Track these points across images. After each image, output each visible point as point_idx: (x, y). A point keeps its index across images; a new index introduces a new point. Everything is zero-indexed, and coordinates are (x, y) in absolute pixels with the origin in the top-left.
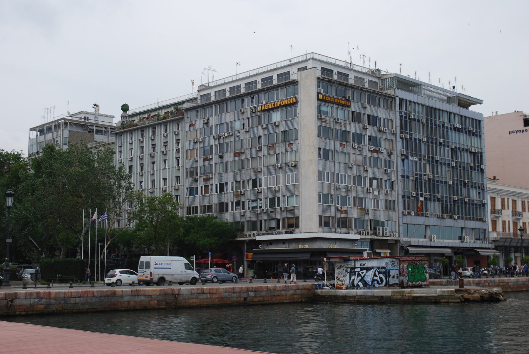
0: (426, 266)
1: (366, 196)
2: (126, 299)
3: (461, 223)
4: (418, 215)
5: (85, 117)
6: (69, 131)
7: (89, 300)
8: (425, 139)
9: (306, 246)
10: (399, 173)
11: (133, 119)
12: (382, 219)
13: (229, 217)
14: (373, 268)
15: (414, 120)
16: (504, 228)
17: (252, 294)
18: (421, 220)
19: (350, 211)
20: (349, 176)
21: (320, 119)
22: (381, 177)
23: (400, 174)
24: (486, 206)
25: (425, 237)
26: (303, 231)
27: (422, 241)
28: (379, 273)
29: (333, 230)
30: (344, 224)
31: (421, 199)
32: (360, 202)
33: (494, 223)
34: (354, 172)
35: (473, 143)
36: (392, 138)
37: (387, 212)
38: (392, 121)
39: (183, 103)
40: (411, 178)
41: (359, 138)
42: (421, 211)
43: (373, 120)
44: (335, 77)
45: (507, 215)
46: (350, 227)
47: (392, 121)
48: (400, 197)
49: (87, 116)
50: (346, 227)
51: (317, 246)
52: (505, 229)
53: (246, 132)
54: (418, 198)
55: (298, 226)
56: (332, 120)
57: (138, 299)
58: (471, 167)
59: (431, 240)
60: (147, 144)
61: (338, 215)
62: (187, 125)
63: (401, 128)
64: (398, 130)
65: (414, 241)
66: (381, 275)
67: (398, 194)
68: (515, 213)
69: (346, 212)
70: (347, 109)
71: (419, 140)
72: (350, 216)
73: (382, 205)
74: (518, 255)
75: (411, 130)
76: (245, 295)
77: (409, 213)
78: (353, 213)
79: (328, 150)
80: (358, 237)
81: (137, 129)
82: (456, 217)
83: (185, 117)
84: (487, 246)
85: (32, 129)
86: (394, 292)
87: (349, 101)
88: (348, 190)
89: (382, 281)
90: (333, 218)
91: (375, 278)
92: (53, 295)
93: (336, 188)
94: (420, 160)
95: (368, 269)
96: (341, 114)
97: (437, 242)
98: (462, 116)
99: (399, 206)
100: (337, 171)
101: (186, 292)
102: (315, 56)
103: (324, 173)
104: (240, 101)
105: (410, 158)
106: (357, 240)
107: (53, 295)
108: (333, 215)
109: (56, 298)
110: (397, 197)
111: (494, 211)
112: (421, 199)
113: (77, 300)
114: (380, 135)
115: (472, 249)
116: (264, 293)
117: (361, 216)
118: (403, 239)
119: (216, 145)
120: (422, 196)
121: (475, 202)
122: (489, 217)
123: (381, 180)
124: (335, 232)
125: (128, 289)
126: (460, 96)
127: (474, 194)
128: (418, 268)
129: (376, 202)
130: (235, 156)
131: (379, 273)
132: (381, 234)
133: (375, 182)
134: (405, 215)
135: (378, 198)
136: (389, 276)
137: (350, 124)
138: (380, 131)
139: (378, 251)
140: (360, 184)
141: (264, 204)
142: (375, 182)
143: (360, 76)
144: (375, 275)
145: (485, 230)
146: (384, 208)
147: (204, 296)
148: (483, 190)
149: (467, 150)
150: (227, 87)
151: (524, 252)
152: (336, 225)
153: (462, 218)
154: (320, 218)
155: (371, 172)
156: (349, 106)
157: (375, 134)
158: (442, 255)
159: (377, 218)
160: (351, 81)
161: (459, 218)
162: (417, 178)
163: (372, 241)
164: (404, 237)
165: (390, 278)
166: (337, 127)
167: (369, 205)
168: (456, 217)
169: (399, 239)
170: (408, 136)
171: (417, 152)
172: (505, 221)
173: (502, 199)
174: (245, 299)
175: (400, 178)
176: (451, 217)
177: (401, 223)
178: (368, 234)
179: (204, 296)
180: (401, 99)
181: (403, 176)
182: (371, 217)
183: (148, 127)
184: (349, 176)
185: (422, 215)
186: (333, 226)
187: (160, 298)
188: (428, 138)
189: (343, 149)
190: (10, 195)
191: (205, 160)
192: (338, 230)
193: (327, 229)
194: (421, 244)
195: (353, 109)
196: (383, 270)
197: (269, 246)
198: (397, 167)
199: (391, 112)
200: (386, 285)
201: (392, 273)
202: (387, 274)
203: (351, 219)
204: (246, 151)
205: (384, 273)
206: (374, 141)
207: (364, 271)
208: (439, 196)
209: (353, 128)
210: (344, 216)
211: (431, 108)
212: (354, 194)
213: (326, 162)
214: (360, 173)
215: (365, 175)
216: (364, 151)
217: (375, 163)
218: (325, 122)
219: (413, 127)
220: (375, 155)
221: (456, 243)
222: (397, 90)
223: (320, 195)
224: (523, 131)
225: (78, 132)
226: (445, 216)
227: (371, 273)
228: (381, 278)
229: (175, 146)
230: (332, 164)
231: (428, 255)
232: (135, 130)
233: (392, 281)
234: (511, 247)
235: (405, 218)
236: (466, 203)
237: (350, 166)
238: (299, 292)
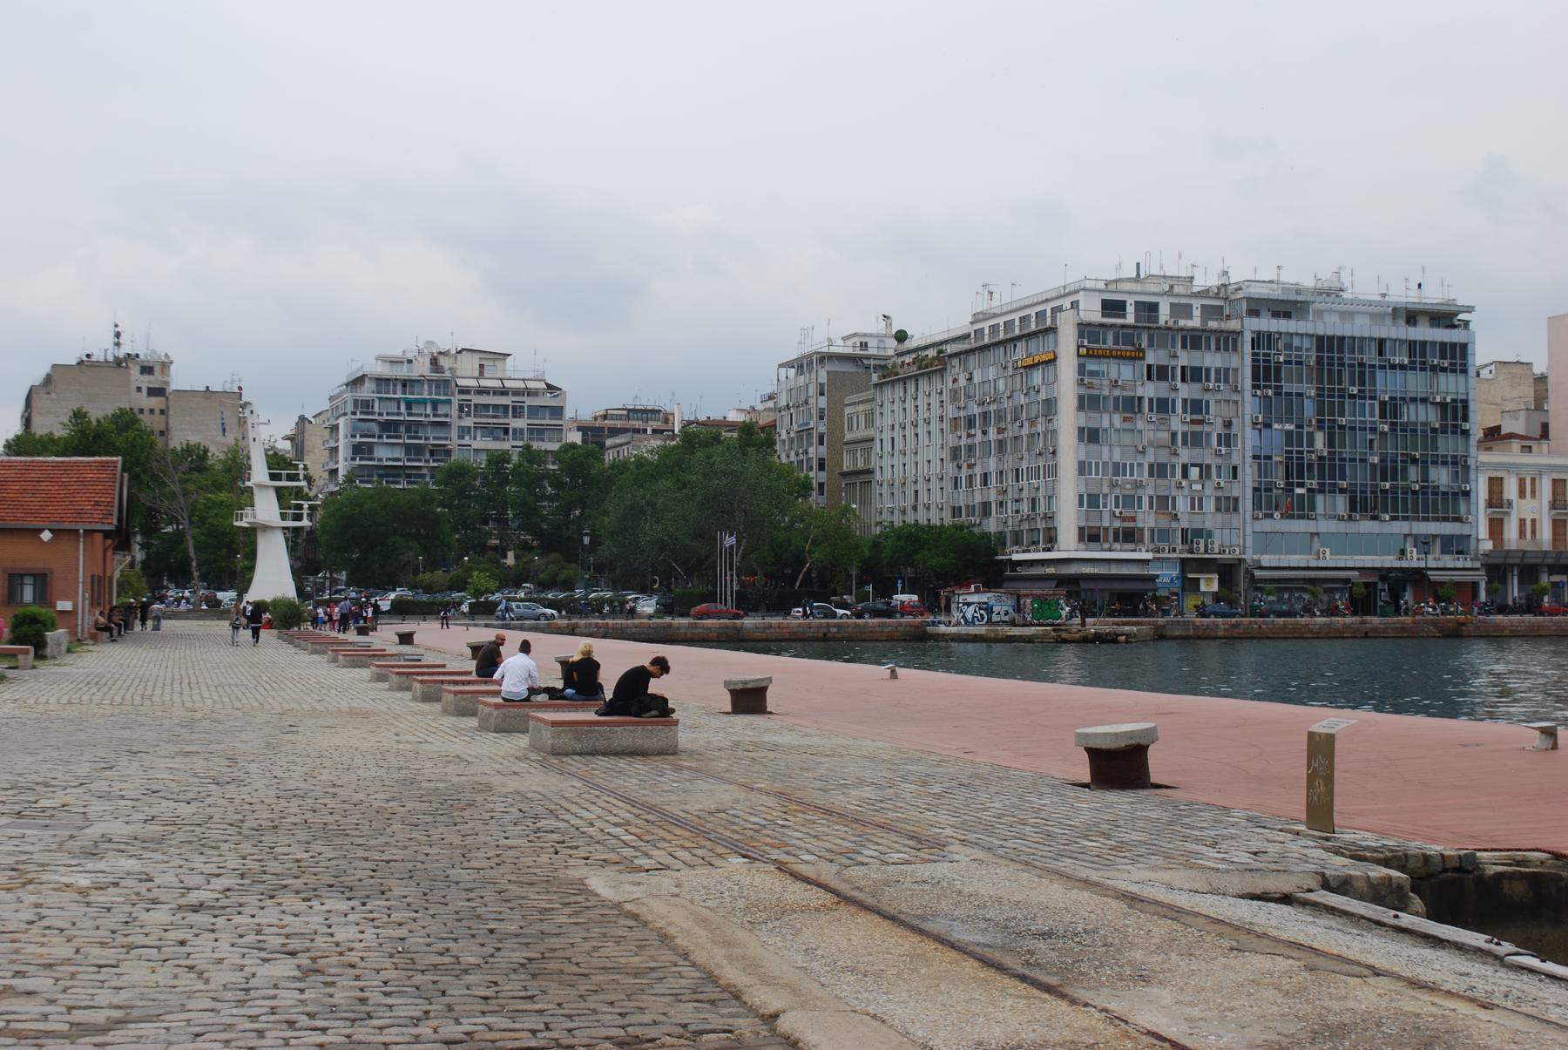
0: (1061, 602)
1: (1174, 492)
2: (683, 631)
3: (1401, 527)
5: (861, 343)
6: (828, 372)
7: (645, 631)
9: (1051, 570)
10: (1247, 453)
11: (926, 353)
12: (1208, 526)
13: (992, 525)
17: (833, 630)
19: (1140, 517)
20: (1140, 465)
21: (1081, 383)
22: (1208, 461)
24: (1473, 495)
28: (980, 609)
29: (1106, 546)
30: (1129, 536)
31: (1299, 491)
32: (1163, 503)
34: (1150, 457)
35: (1448, 386)
36: (1235, 397)
37: (1219, 516)
38: (1236, 370)
39: (946, 342)
41: (1163, 406)
42: (1303, 509)
46: (1142, 541)
47: (1236, 370)
49: (864, 340)
50: (1132, 541)
51: (1073, 570)
52: (1525, 533)
56: (1106, 382)
57: (694, 631)
58: (1434, 430)
61: (1117, 524)
62: (950, 380)
64: (1248, 383)
65: (1266, 560)
66: (982, 612)
67: (1244, 487)
69: (1133, 519)
70: (1137, 362)
71: (1300, 395)
72: (1140, 525)
73: (1210, 505)
76: (825, 631)
78: (1147, 519)
79: (1098, 430)
80: (1149, 556)
81: (898, 380)
83: (949, 367)
84: (1469, 564)
85: (781, 366)
88: (1138, 485)
89: (983, 618)
90: (1106, 529)
92: (610, 626)
93: (1113, 485)
94: (1299, 426)
95: (969, 604)
96: (1126, 372)
99: (1247, 504)
100: (1117, 458)
101: (749, 626)
102: (1089, 285)
103: (1090, 463)
104: (1002, 349)
105: (1276, 426)
106: (1149, 560)
107: (610, 626)
108: (1106, 523)
109: (612, 628)
110: (1244, 489)
112: (1299, 491)
113: (634, 630)
114: (1207, 396)
115: (1418, 571)
116: (850, 629)
117: (1164, 523)
118: (1249, 556)
121: (1442, 489)
123: (1208, 467)
124: (1110, 550)
125: (646, 621)
126: (1409, 306)
127: (1441, 477)
128: (1049, 604)
130: (998, 433)
131: (980, 609)
132: (1202, 550)
134: (1257, 519)
135: (1200, 494)
136: (992, 612)
137: (1143, 384)
138: (1208, 390)
141: (1025, 507)
143: (1183, 301)
144: (975, 611)
146: (1213, 509)
147: (772, 630)
148: (1467, 468)
149: (1424, 400)
150: (1016, 317)
151: (1516, 573)
152: (1111, 538)
154: (1081, 530)
155: (1185, 455)
156: (1143, 358)
157: (1197, 396)
158: (1347, 581)
162: (1289, 459)
163: (1183, 561)
165: (994, 615)
166: (1117, 393)
167: (1182, 505)
169: (1244, 556)
172: (1525, 520)
173: (1520, 479)
174: (825, 635)
178: (1174, 550)
179: (772, 630)
182: (1184, 524)
183: (910, 377)
184: (1140, 465)
186: (1106, 540)
187: (720, 631)
189: (1128, 425)
190: (586, 534)
191: (969, 436)
192: (1117, 546)
193: (1093, 545)
197: (1031, 569)
198: (1243, 443)
201: (996, 609)
202: (990, 610)
203: (1142, 530)
204: (1009, 427)
206: (1196, 406)
208: (1344, 484)
209: (1149, 390)
210: (1131, 525)
212: (1150, 491)
213: (1093, 447)
214: (1163, 456)
215: (1174, 460)
216: (1172, 423)
217: (1195, 440)
218: (1093, 388)
220: (1197, 428)
221: (1390, 561)
223: (1081, 497)
225: (844, 373)
227: (972, 608)
228: (981, 615)
230: (1105, 450)
231: (1313, 581)
232: (896, 380)
233: (995, 618)
235: (1256, 522)
236: (1415, 492)
237: (1140, 449)
238: (901, 629)
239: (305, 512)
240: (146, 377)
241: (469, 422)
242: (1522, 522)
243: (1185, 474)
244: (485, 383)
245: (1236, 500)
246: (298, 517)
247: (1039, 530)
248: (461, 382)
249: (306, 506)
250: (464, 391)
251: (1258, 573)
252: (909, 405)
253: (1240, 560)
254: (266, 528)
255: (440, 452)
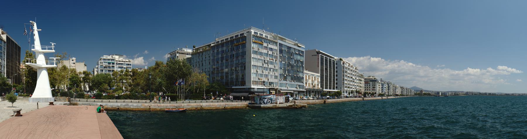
3: (297, 83)
4: (284, 80)
8: (287, 57)
14: (267, 98)
15: (284, 50)
16: (309, 85)
17: (227, 106)
18: (285, 82)
23: (279, 67)
25: (286, 87)
26: (247, 85)
27: (285, 88)
31: (285, 75)
33: (306, 84)
38: (277, 50)
40: (283, 69)
42: (285, 79)
43: (271, 49)
44: (259, 35)
45: (310, 81)
48: (279, 75)
53: (230, 53)
54: (284, 75)
55: (245, 84)
59: (288, 88)
60: (201, 58)
63: (280, 52)
65: (282, 88)
68: (312, 81)
74: (313, 93)
75: (283, 53)
76: (225, 106)
77: (282, 80)
82: (295, 81)
86: (273, 105)
87: (263, 42)
89: (270, 102)
91: (268, 101)
97: (289, 89)
98: (298, 50)
99: (279, 77)
105: (282, 62)
111: (306, 80)
119: (235, 54)
120: (286, 74)
122: (305, 82)
129: (272, 76)
131: (269, 99)
133: (272, 70)
136: (272, 100)
139: (271, 92)
140: (266, 70)
142: (272, 70)
144: (267, 100)
145: (303, 86)
153: (297, 82)
156: (263, 44)
159: (271, 81)
160: (264, 37)
161: (296, 82)
164: (280, 87)
168: (295, 81)
170: (282, 55)
171: (284, 60)
175: (279, 68)
176: (294, 81)
177: (279, 83)
180: (280, 43)
181: (280, 68)
185: (285, 80)
188: (288, 56)
192: (259, 85)
194: (285, 89)
195: (264, 45)
196: (270, 99)
199: (277, 47)
200: (271, 103)
205: (270, 100)
207: (264, 99)
211: (289, 47)
219: (283, 52)
222: (278, 40)
224: (316, 55)
226: (292, 81)
228: (269, 101)
229: (209, 58)
234: (310, 91)
239: (55, 62)
240: (73, 61)
241: (117, 66)
242: (309, 83)
243: (270, 70)
244: (120, 60)
245: (277, 76)
246: (53, 64)
247: (239, 82)
248: (116, 60)
249: (55, 59)
250: (117, 61)
251: (282, 91)
252: (201, 58)
253: (277, 88)
254: (41, 69)
255: (113, 71)
